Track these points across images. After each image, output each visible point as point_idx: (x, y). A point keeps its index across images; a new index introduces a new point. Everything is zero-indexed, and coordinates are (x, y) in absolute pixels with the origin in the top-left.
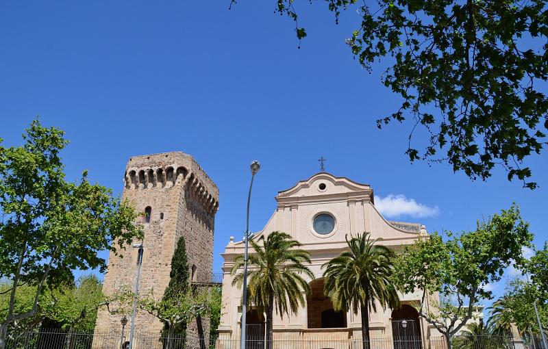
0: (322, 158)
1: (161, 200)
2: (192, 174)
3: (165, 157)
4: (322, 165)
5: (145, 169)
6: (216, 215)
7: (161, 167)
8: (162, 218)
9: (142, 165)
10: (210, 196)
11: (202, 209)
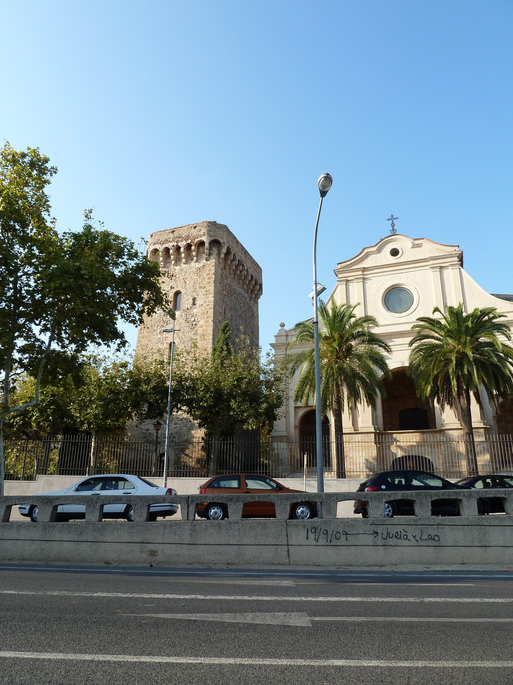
0: (392, 216)
1: (192, 282)
2: (228, 248)
3: (193, 230)
4: (393, 225)
5: (170, 245)
6: (261, 301)
7: (189, 241)
8: (194, 304)
9: (167, 241)
10: (252, 276)
11: (243, 293)
